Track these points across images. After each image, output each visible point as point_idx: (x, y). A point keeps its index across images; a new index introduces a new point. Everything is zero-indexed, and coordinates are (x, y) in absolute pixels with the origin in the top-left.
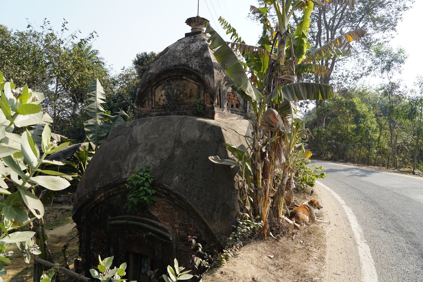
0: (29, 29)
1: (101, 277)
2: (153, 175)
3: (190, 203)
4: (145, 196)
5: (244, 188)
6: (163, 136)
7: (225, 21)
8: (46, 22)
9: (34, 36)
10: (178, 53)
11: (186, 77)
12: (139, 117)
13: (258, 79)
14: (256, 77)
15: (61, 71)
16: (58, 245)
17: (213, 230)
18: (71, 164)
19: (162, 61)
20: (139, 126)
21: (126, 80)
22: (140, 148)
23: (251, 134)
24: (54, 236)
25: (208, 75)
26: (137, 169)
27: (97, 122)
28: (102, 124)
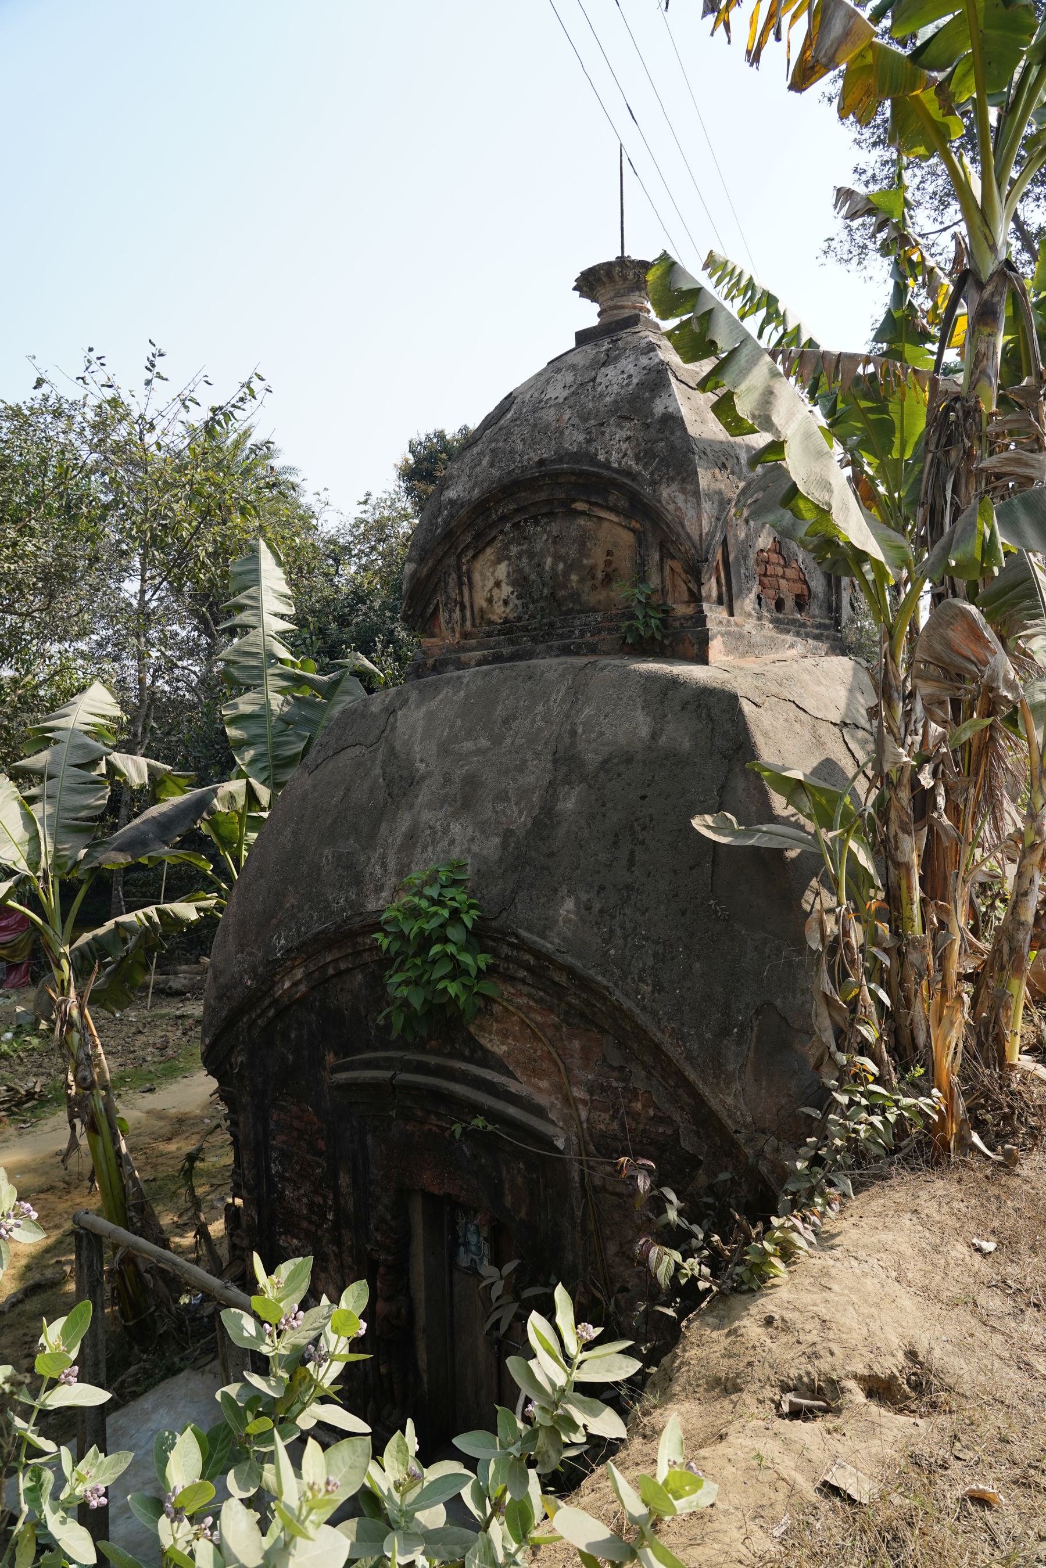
0: (38, 393)
1: (268, 1340)
2: (479, 895)
3: (627, 1004)
4: (452, 977)
5: (848, 945)
6: (509, 740)
7: (730, 268)
8: (94, 360)
9: (57, 414)
10: (552, 411)
11: (588, 502)
12: (419, 671)
13: (882, 489)
14: (872, 479)
15: (152, 529)
16: (172, 1147)
17: (723, 1114)
18: (192, 860)
19: (493, 451)
20: (418, 707)
21: (379, 541)
22: (424, 793)
23: (864, 712)
24: (159, 1115)
25: (674, 487)
26: (417, 876)
27: (268, 702)
28: (286, 709)
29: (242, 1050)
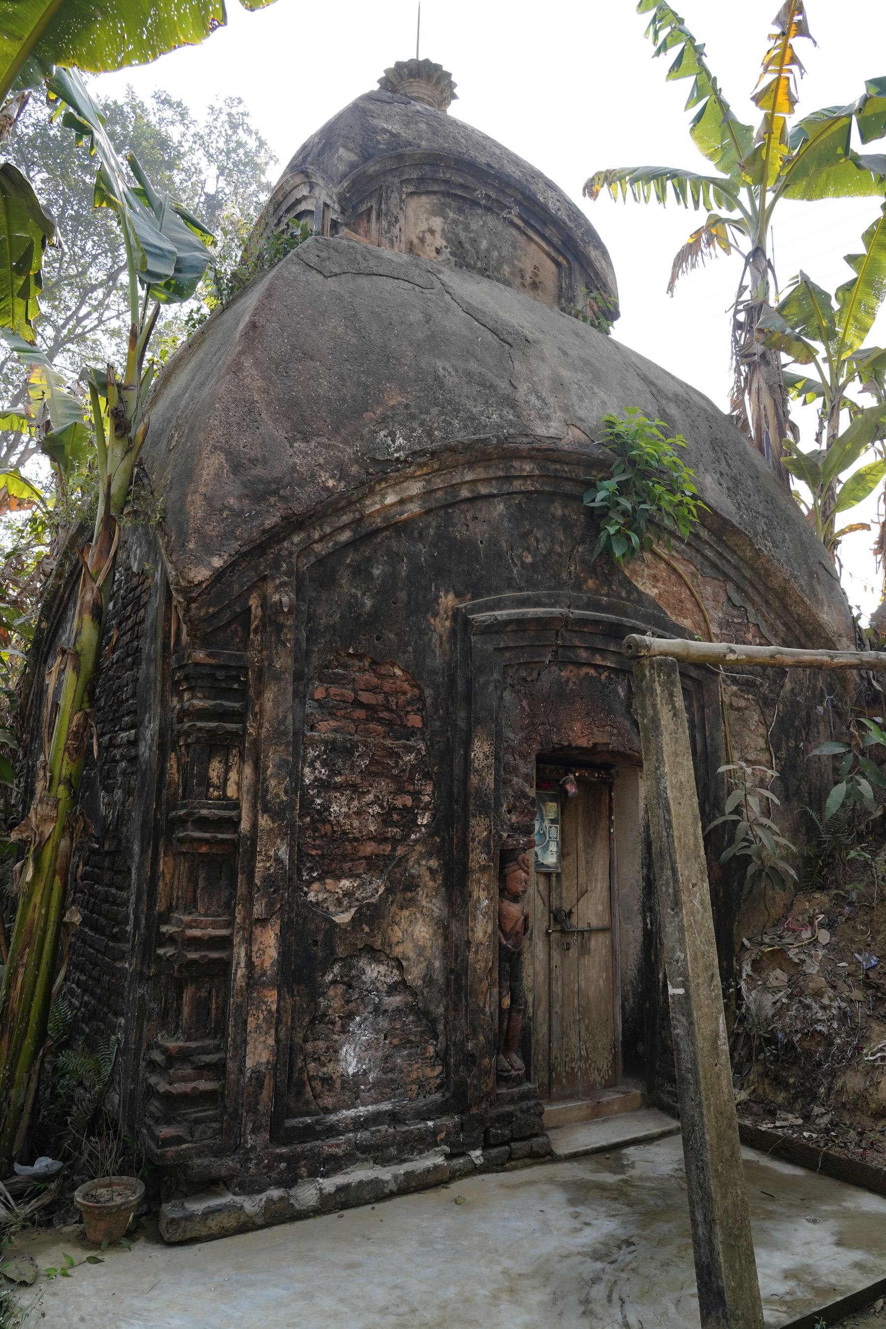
29: (284, 584)
